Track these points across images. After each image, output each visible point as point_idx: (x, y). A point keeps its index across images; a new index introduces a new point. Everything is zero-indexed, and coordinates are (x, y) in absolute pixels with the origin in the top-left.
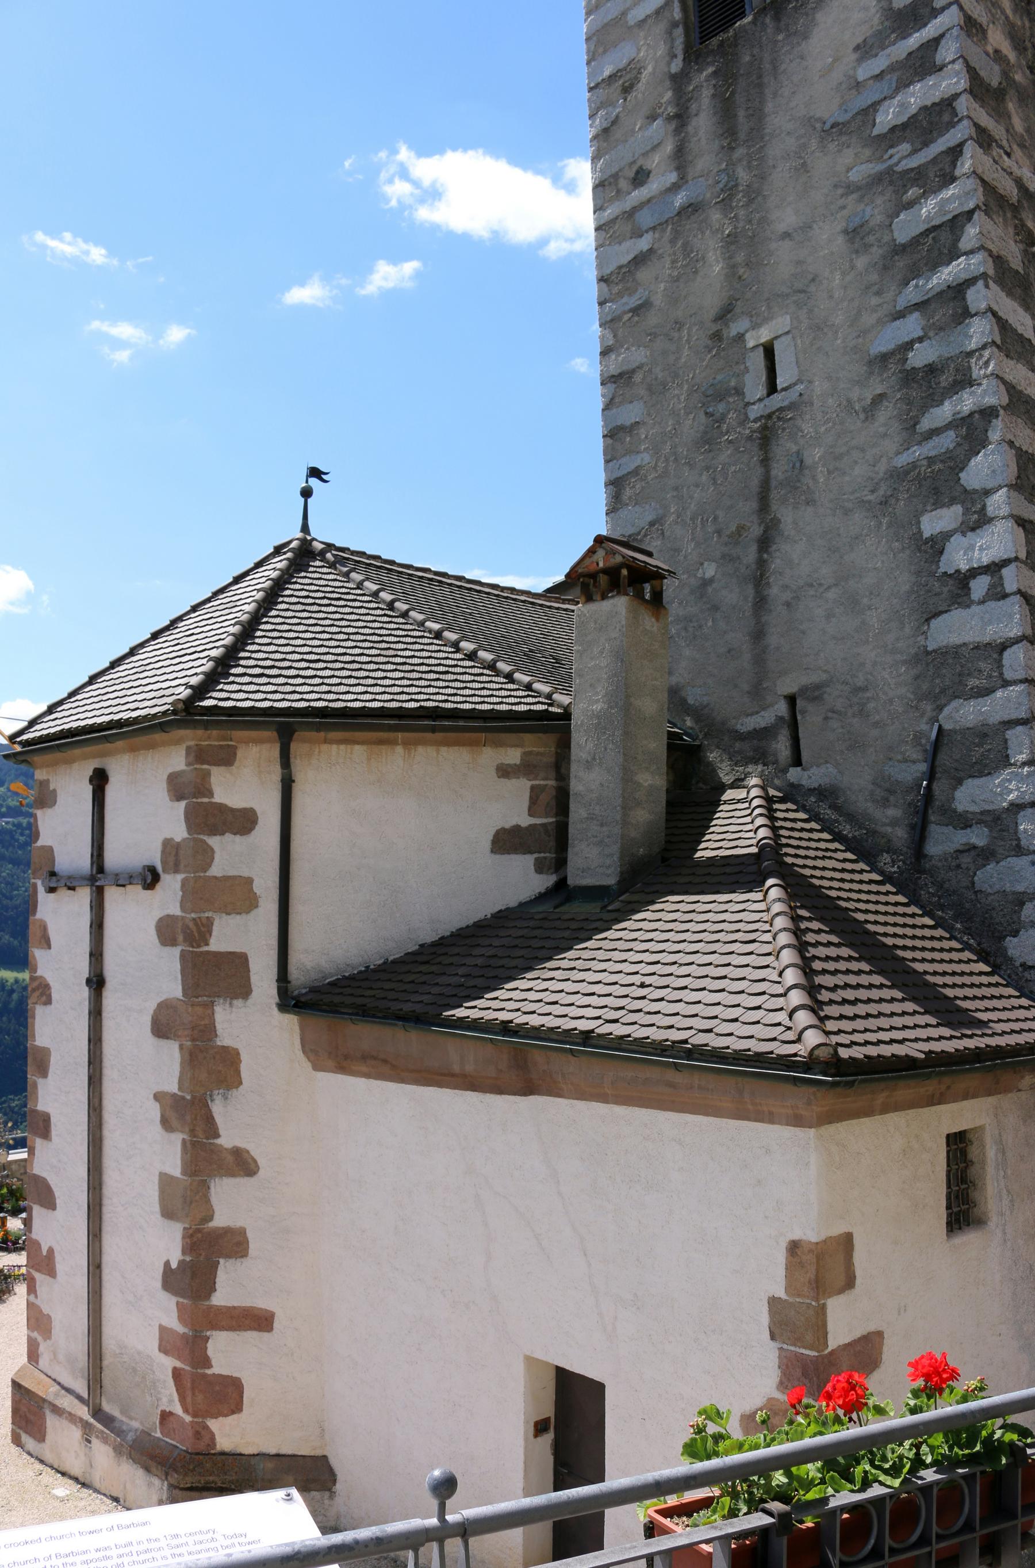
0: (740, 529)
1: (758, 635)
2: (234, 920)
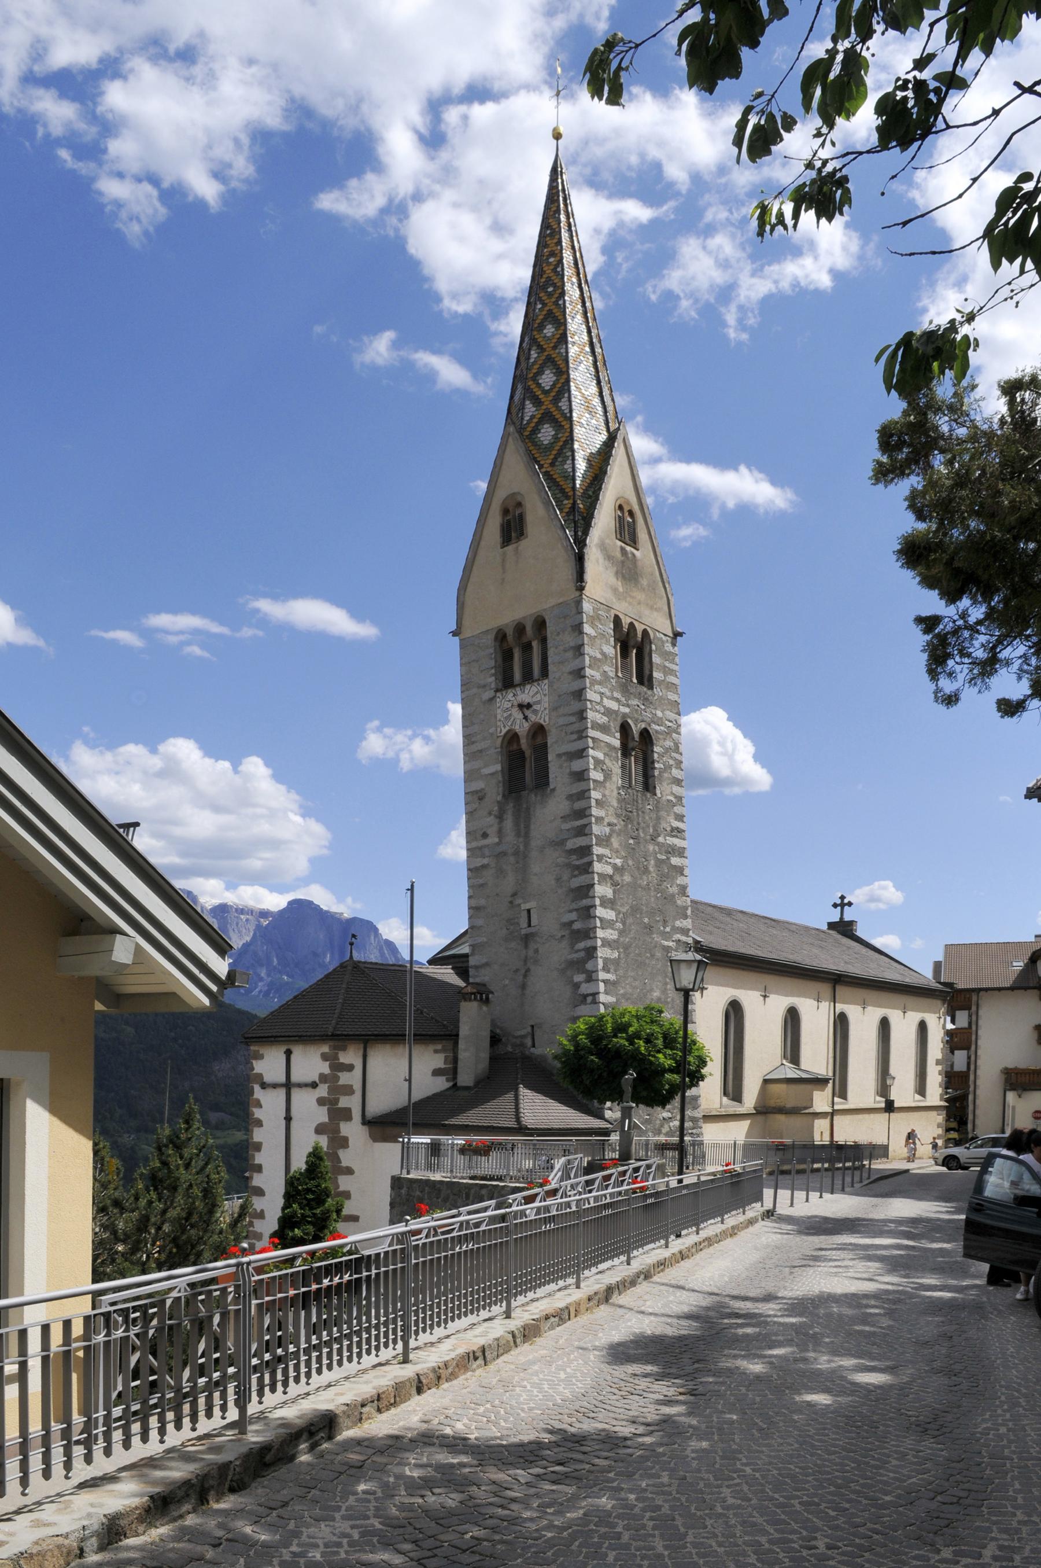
2: (347, 1097)
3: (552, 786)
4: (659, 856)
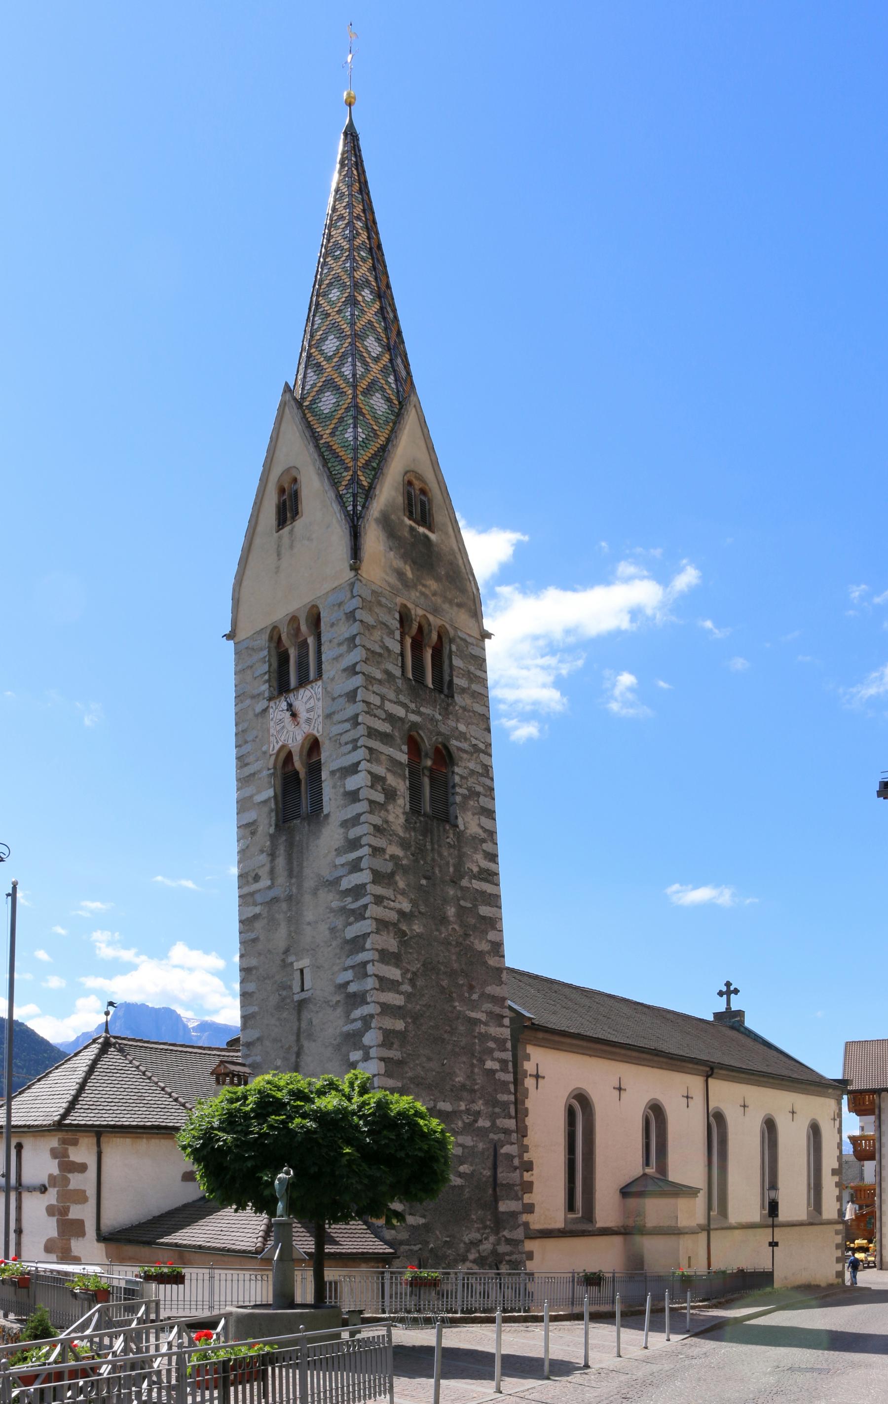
0: (290, 1047)
2: (79, 1207)
3: (325, 811)
4: (462, 903)
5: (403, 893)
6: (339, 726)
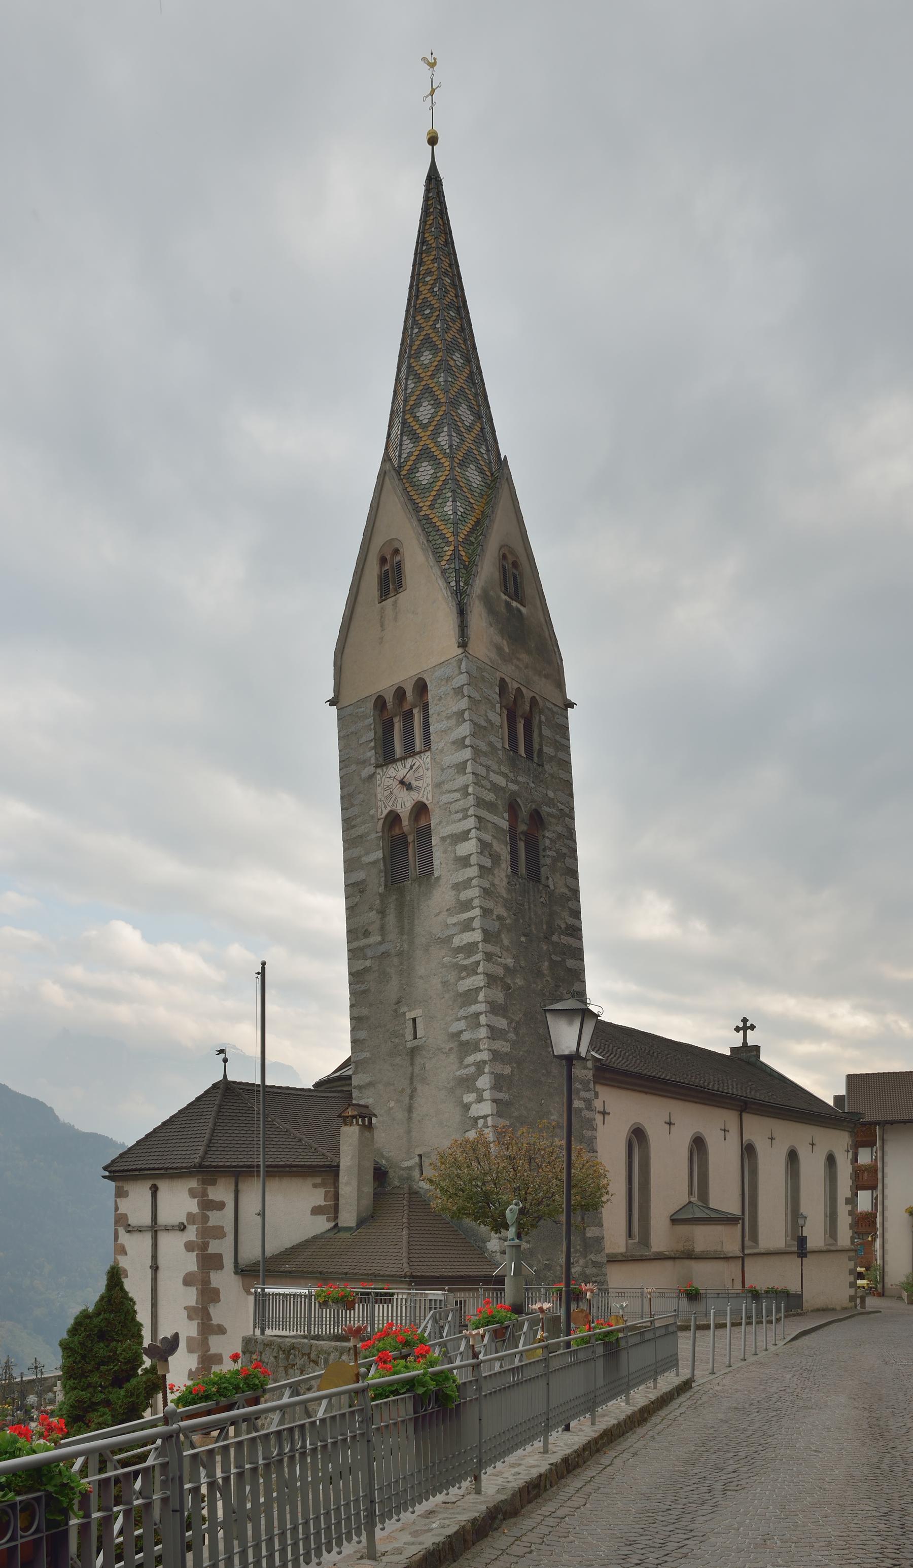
0: (403, 1090)
1: (409, 1132)
3: (436, 875)
4: (553, 957)
5: (507, 950)
6: (447, 795)
